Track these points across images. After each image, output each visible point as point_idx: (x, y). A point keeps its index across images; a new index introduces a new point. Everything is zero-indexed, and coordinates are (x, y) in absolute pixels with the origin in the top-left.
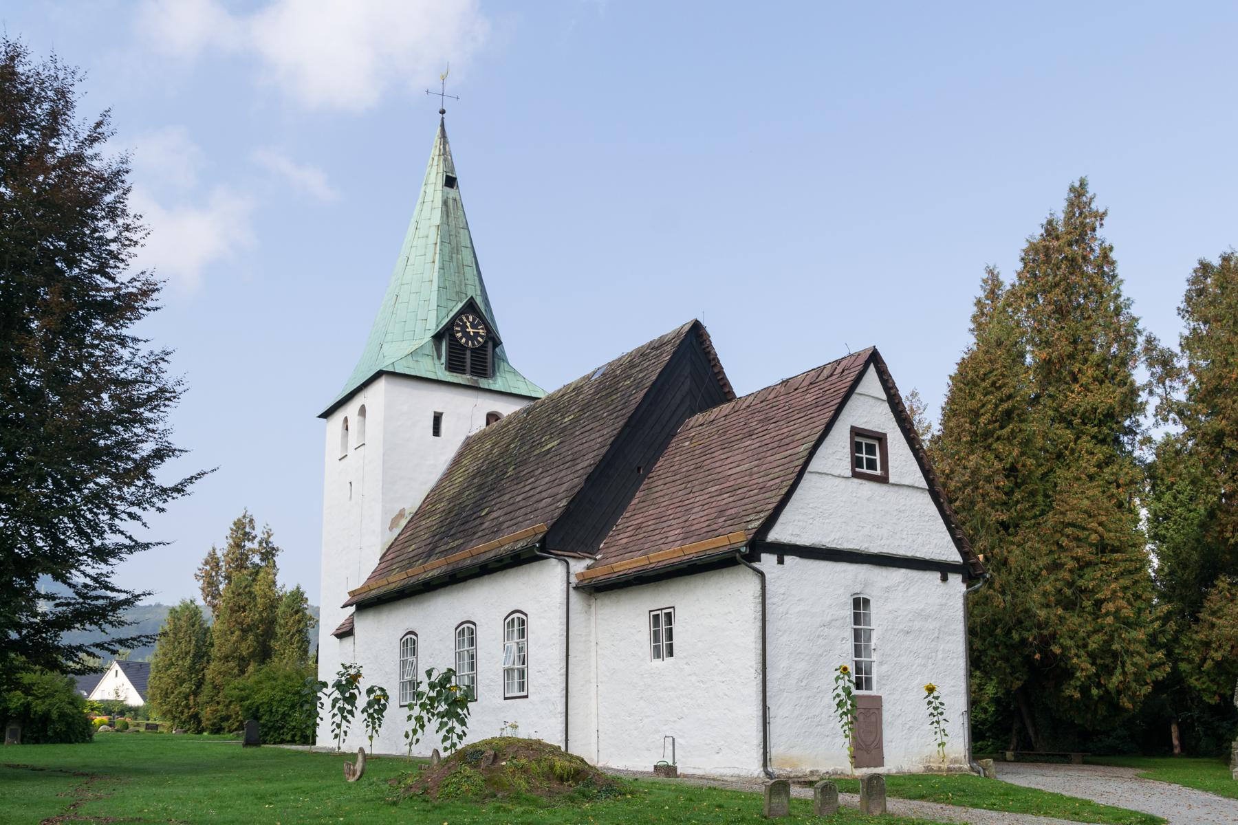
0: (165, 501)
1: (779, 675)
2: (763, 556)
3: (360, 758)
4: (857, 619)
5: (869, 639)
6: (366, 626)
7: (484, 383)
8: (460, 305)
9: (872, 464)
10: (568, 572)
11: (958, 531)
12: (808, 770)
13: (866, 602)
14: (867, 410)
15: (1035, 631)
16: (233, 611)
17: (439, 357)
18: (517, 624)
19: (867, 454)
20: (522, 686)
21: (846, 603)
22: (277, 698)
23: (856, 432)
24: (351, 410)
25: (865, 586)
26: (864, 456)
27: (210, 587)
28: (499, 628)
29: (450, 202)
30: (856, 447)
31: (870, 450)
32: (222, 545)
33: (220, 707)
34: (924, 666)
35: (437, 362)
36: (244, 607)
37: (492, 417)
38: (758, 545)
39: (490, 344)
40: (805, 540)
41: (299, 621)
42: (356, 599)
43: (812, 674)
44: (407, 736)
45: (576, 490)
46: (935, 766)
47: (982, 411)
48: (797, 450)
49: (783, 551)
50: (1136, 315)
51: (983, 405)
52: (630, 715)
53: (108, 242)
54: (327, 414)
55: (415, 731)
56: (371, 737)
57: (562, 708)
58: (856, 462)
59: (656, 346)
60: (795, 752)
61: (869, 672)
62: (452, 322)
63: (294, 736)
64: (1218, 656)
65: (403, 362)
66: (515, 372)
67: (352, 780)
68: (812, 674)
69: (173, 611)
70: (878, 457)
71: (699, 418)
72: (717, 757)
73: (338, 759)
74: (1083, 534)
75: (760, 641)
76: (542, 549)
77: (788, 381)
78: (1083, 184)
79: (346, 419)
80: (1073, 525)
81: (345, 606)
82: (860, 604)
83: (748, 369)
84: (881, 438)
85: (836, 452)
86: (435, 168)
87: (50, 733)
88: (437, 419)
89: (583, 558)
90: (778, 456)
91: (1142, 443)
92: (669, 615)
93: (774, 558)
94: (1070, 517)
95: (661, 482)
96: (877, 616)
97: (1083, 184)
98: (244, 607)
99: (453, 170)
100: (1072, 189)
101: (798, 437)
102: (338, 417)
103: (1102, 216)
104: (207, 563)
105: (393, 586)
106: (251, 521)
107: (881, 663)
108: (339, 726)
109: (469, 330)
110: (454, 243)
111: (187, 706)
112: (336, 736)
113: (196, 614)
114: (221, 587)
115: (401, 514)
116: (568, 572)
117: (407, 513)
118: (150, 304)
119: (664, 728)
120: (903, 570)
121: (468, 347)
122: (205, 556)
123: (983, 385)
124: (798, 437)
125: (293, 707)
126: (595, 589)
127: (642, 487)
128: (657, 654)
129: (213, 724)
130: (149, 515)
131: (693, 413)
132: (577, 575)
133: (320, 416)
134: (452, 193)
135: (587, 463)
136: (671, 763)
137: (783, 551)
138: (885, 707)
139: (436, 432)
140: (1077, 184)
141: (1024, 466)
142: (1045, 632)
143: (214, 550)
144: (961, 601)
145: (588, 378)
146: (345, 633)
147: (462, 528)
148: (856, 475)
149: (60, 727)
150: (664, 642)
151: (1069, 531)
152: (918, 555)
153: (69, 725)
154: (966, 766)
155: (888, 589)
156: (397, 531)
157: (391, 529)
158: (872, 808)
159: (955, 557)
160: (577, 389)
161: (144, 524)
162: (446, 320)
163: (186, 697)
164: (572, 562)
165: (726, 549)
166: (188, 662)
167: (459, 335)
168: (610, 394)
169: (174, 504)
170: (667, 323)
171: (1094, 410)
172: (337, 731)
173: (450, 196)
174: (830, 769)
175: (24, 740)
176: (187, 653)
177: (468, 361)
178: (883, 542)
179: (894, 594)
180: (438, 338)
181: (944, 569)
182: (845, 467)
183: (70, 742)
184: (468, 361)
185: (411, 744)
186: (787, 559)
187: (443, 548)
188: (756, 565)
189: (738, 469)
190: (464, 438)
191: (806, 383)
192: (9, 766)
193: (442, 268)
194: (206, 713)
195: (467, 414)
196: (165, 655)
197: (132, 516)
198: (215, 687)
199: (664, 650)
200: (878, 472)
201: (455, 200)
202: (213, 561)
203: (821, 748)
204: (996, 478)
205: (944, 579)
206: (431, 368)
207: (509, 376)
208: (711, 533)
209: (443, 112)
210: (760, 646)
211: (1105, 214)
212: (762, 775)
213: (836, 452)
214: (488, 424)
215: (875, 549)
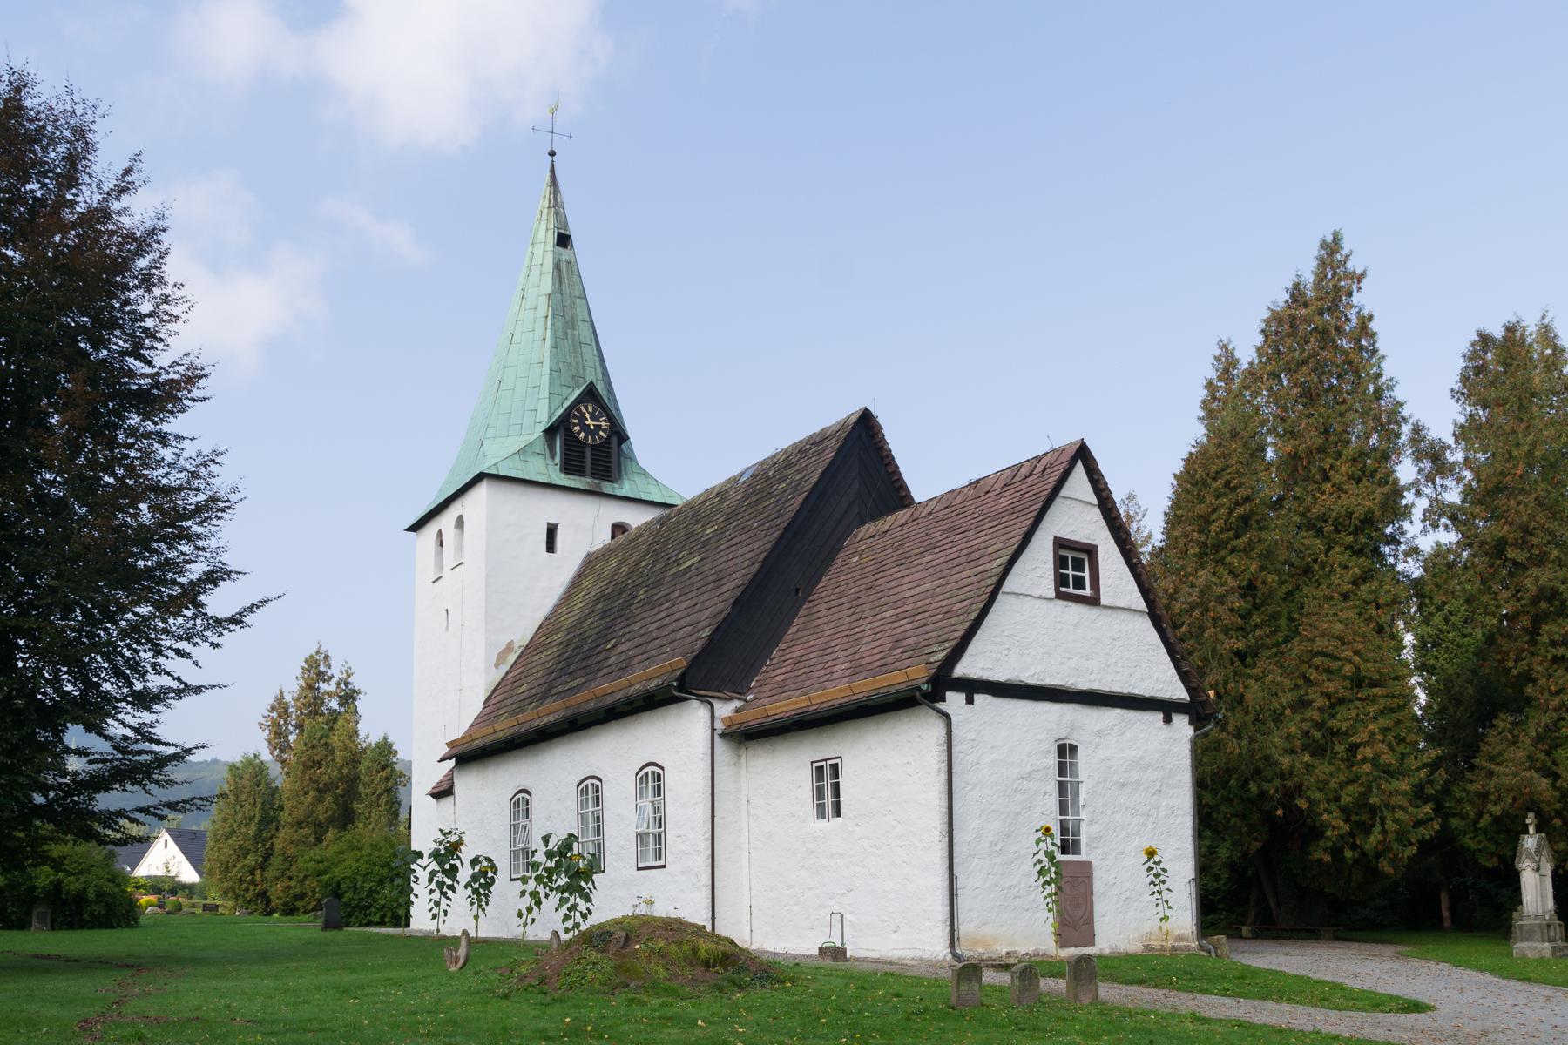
0: (221, 634)
1: (967, 838)
2: (949, 695)
3: (464, 942)
4: (1062, 770)
5: (1077, 794)
6: (469, 784)
7: (608, 487)
8: (577, 392)
9: (1079, 583)
11: (1184, 663)
12: (1004, 951)
13: (1074, 748)
14: (1076, 517)
15: (1277, 782)
16: (306, 767)
17: (553, 456)
18: (652, 779)
19: (1074, 571)
20: (658, 854)
22: (362, 871)
23: (1060, 544)
24: (446, 521)
25: (1073, 729)
26: (1070, 572)
28: (630, 784)
29: (564, 266)
30: (1061, 562)
31: (1078, 565)
32: (292, 688)
33: (292, 883)
34: (1144, 825)
35: (549, 461)
36: (319, 763)
37: (618, 529)
38: (942, 682)
39: (615, 440)
40: (999, 675)
41: (387, 779)
42: (455, 751)
43: (1008, 836)
44: (520, 915)
46: (1156, 944)
49: (971, 688)
50: (1400, 398)
51: (1215, 510)
52: (789, 887)
53: (143, 317)
54: (416, 527)
58: (1061, 581)
60: (988, 930)
61: (1077, 833)
62: (568, 414)
63: (383, 917)
64: (1497, 810)
65: (510, 463)
66: (645, 474)
67: (454, 969)
68: (1008, 836)
69: (233, 767)
70: (1087, 574)
71: (870, 528)
72: (895, 936)
73: (437, 944)
74: (1334, 665)
75: (946, 796)
76: (681, 688)
77: (977, 482)
78: (1337, 238)
79: (440, 533)
80: (1323, 654)
81: (442, 760)
82: (1066, 752)
83: (928, 471)
84: (1091, 551)
85: (1037, 568)
86: (544, 224)
87: (86, 917)
88: (552, 531)
89: (731, 699)
90: (966, 574)
91: (1407, 554)
92: (835, 768)
93: (962, 697)
94: (1320, 644)
96: (1087, 766)
97: (1337, 238)
98: (319, 763)
99: (566, 226)
100: (1324, 245)
101: (991, 550)
102: (431, 530)
104: (273, 709)
105: (500, 735)
106: (326, 657)
107: (1091, 823)
108: (437, 904)
109: (589, 422)
110: (568, 317)
111: (253, 882)
112: (434, 916)
113: (261, 771)
114: (291, 738)
115: (509, 648)
116: (713, 717)
117: (516, 646)
118: (196, 393)
119: (831, 902)
120: (1118, 711)
121: (588, 445)
123: (1216, 485)
124: (991, 550)
125: (381, 882)
126: (747, 735)
127: (801, 613)
128: (821, 813)
129: (285, 904)
130: (201, 651)
132: (723, 720)
134: (565, 254)
135: (735, 582)
136: (839, 945)
137: (971, 688)
138: (1097, 874)
139: (551, 547)
140: (1329, 239)
141: (1264, 583)
142: (1289, 783)
143: (282, 693)
144: (1188, 746)
145: (734, 480)
146: (443, 792)
147: (584, 664)
148: (1060, 596)
149: (99, 909)
150: (829, 799)
151: (1318, 661)
152: (1136, 692)
154: (1194, 944)
155: (1099, 733)
156: (505, 668)
157: (497, 666)
159: (1180, 693)
160: (721, 493)
161: (195, 663)
163: (252, 872)
164: (717, 705)
165: (903, 687)
166: (253, 829)
167: (577, 428)
168: (760, 501)
169: (229, 639)
170: (834, 413)
171: (1350, 515)
172: (435, 910)
174: (1030, 949)
175: (55, 925)
180: (550, 432)
181: (1167, 708)
182: (1048, 586)
183: (112, 927)
185: (525, 925)
186: (978, 698)
187: (560, 688)
188: (940, 705)
189: (917, 590)
192: (37, 956)
193: (555, 347)
194: (276, 891)
195: (588, 525)
196: (225, 820)
198: (286, 859)
199: (830, 809)
200: (1088, 592)
201: (569, 263)
202: (280, 706)
203: (1019, 924)
205: (1168, 720)
207: (637, 479)
208: (886, 667)
209: (552, 154)
211: (1363, 275)
212: (949, 957)
213: (1037, 568)
214: (613, 537)
215: (1083, 685)
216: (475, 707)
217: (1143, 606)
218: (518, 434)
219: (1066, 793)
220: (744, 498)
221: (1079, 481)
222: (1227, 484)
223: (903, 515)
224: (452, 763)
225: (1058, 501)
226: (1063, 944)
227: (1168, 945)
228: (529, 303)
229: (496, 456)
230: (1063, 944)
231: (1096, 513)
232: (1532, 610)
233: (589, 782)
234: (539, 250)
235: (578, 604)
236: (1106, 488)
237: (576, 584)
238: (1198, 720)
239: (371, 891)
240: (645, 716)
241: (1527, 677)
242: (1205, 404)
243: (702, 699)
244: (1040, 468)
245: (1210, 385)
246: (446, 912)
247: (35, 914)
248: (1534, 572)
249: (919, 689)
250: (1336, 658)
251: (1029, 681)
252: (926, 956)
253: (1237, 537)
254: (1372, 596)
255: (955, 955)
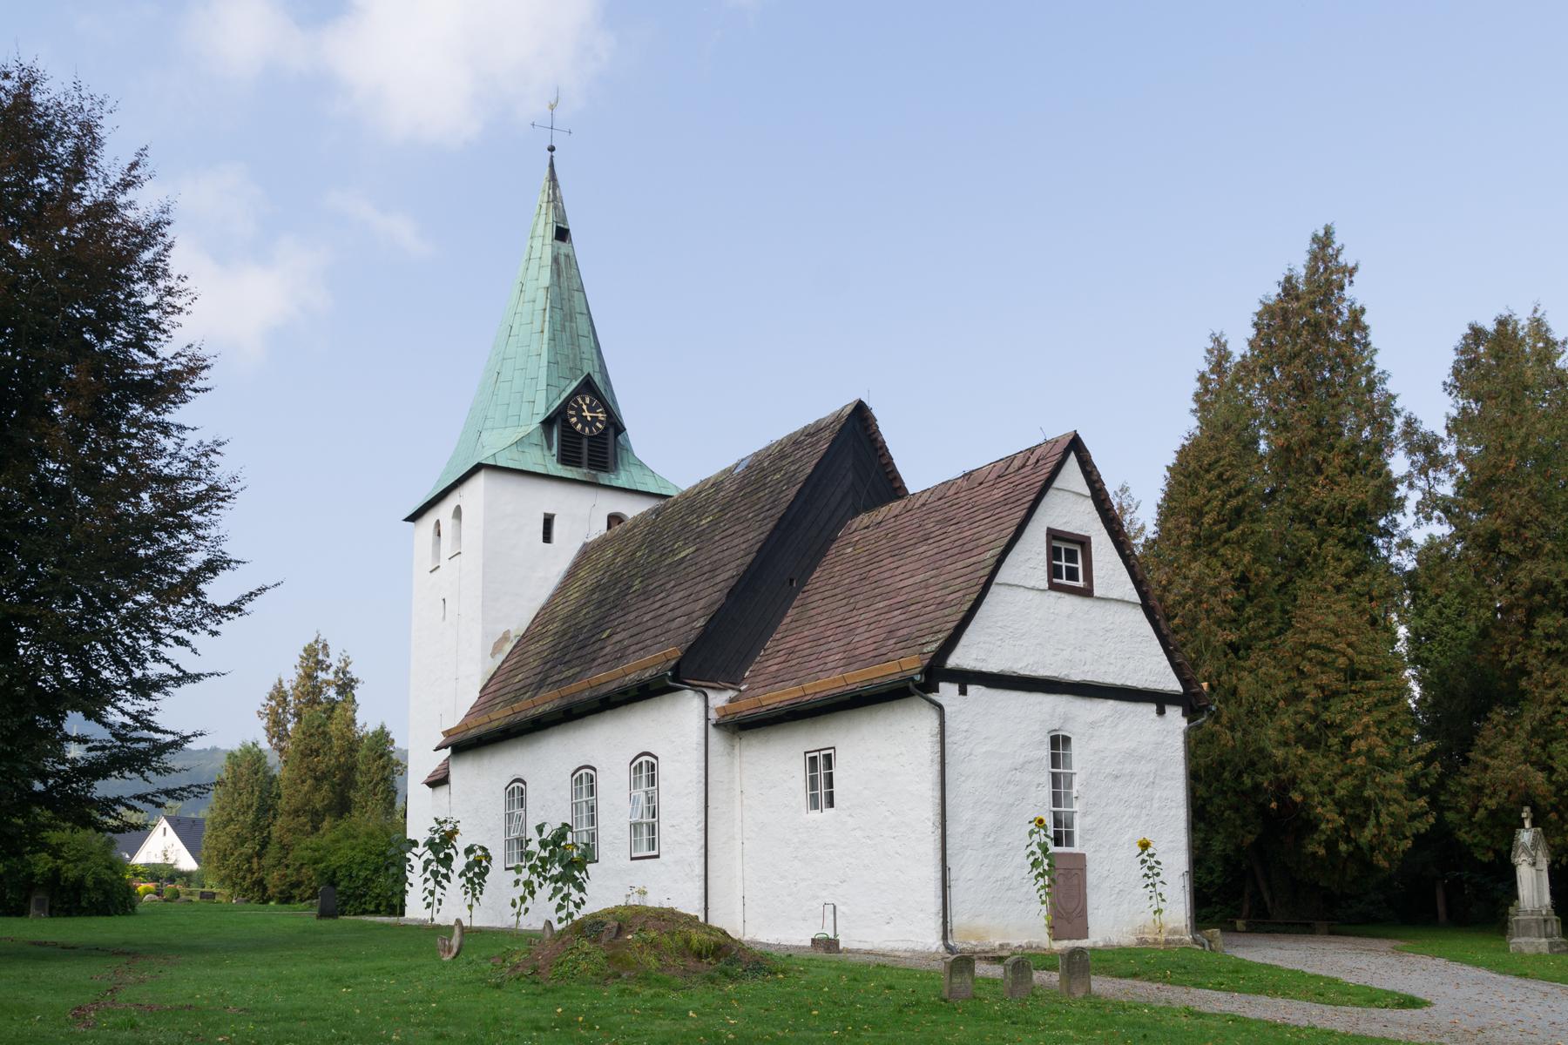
0: (219, 622)
2: (942, 685)
3: (457, 931)
4: (1055, 761)
5: (1070, 786)
7: (604, 478)
8: (575, 384)
9: (1072, 574)
10: (707, 707)
11: (1177, 655)
12: (997, 944)
13: (1067, 740)
14: (1069, 509)
15: (1271, 775)
17: (550, 447)
18: (646, 769)
19: (1067, 563)
20: (652, 844)
21: (1041, 742)
22: (358, 860)
23: (1053, 535)
24: (444, 511)
26: (1064, 564)
27: (276, 726)
29: (562, 259)
30: (1054, 554)
31: (1071, 557)
32: (290, 676)
33: (289, 872)
34: (1137, 817)
35: (547, 453)
37: (614, 519)
38: (935, 673)
39: (611, 432)
40: (992, 666)
41: (384, 768)
42: (451, 740)
43: (1000, 828)
44: (514, 905)
45: (716, 607)
46: (1150, 937)
47: (1206, 509)
48: (982, 557)
49: (965, 679)
50: (1393, 391)
51: (1208, 502)
53: (147, 309)
54: (414, 517)
55: (523, 899)
56: (470, 907)
57: (700, 870)
58: (1054, 572)
59: (812, 432)
60: (981, 922)
61: (1070, 824)
66: (641, 465)
67: (447, 958)
68: (1000, 828)
69: (231, 755)
70: (1080, 566)
71: (864, 519)
72: (887, 927)
74: (1327, 658)
75: (938, 787)
77: (970, 473)
78: (1328, 232)
80: (1317, 646)
82: (1059, 743)
83: (922, 463)
84: (1084, 543)
86: (543, 217)
87: (84, 904)
88: (548, 522)
89: (725, 689)
90: (959, 565)
91: (1400, 546)
92: (828, 758)
94: (1313, 636)
95: (818, 597)
96: (1080, 757)
97: (1328, 232)
99: (565, 220)
100: (1315, 239)
101: (984, 541)
102: (429, 520)
103: (1352, 271)
104: (271, 698)
105: (495, 724)
106: (325, 646)
107: (1085, 815)
108: (432, 893)
109: (586, 413)
110: (566, 308)
111: (250, 870)
112: (429, 905)
113: (259, 760)
115: (505, 637)
116: (707, 707)
118: (198, 384)
120: (1111, 702)
121: (585, 436)
122: (270, 689)
123: (1208, 477)
124: (984, 541)
125: (376, 870)
126: (740, 726)
128: (814, 804)
129: (281, 892)
130: (200, 639)
131: (857, 514)
132: (717, 710)
133: (407, 520)
134: (564, 248)
135: (729, 575)
136: (831, 936)
137: (965, 679)
138: (1090, 866)
139: (547, 538)
140: (1321, 233)
141: (1257, 575)
142: (1283, 776)
143: (280, 682)
144: (1181, 739)
145: (730, 471)
146: (438, 781)
148: (1053, 587)
149: (97, 896)
150: (822, 790)
151: (1311, 653)
153: (106, 893)
154: (1188, 938)
155: (1093, 725)
156: (500, 658)
157: (493, 655)
158: (1074, 989)
159: (1173, 684)
160: (716, 484)
162: (559, 402)
164: (711, 695)
165: (897, 677)
166: (250, 817)
167: (574, 420)
169: (230, 627)
170: (828, 404)
171: (1342, 507)
172: (430, 899)
173: (562, 251)
174: (1024, 942)
176: (249, 807)
177: (585, 451)
178: (1086, 668)
179: (1103, 733)
180: (548, 423)
181: (1160, 700)
182: (1041, 577)
183: (108, 914)
184: (585, 451)
185: (519, 914)
186: (971, 689)
187: (556, 678)
188: (933, 696)
189: (911, 581)
190: (579, 545)
191: (993, 476)
193: (552, 339)
194: (273, 879)
195: (584, 515)
196: (223, 808)
197: (180, 641)
198: (283, 847)
199: (823, 800)
200: (1081, 583)
202: (279, 695)
203: (1012, 917)
204: (1223, 590)
205: (1161, 712)
206: (540, 461)
207: (634, 470)
208: (879, 658)
209: (552, 149)
210: (938, 794)
211: (1355, 269)
212: (942, 949)
214: (609, 527)
215: (1076, 676)
216: (472, 696)
217: (1136, 598)
218: (515, 425)
219: (1059, 785)
220: (739, 489)
221: (1072, 473)
222: (1220, 476)
223: (896, 506)
224: (448, 752)
225: (1051, 492)
226: (1056, 937)
227: (1162, 938)
228: (528, 295)
229: (494, 447)
230: (1056, 937)
231: (1089, 505)
232: (1526, 603)
233: (643, 759)
234: (537, 243)
235: (574, 594)
236: (1099, 480)
237: (572, 574)
238: (1191, 712)
239: (366, 879)
240: (639, 706)
241: (1522, 670)
242: (1197, 397)
243: (693, 687)
244: (1033, 460)
245: (1202, 378)
246: (440, 901)
247: (33, 901)
248: (1528, 565)
249: (912, 679)
250: (1330, 651)
251: (1022, 672)
252: (918, 948)
253: (1230, 528)
254: (1366, 589)
255: (947, 947)
